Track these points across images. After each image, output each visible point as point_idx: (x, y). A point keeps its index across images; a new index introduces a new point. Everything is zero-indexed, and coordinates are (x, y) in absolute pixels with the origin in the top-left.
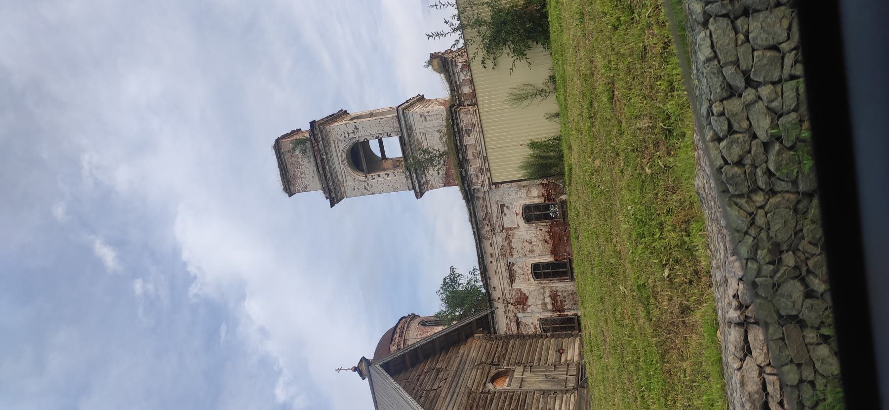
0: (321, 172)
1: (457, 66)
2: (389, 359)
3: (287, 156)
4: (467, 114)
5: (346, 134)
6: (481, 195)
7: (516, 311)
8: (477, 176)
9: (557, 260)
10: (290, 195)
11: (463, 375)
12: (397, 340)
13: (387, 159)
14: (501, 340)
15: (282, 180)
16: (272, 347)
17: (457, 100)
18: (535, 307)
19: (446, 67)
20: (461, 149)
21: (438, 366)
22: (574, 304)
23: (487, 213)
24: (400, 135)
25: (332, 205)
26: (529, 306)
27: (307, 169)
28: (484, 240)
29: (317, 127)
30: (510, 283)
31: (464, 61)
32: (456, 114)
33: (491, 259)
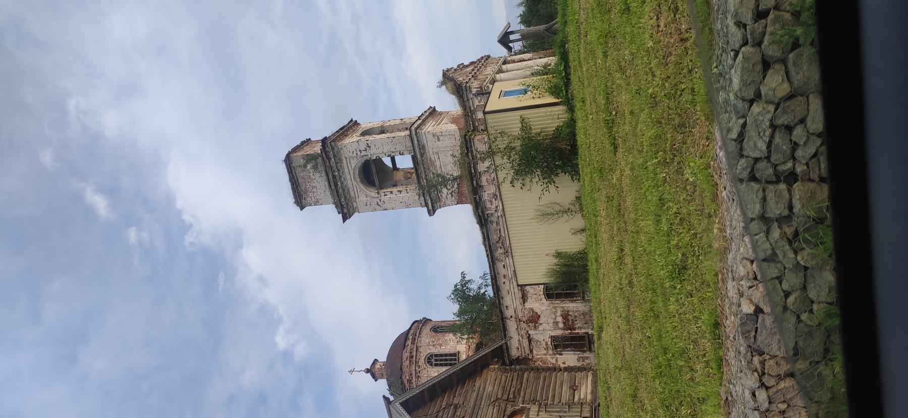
0: (333, 187)
2: (408, 397)
3: (298, 170)
5: (358, 151)
6: (494, 219)
7: (528, 329)
10: (302, 209)
11: (480, 413)
12: (409, 347)
13: (398, 169)
14: (516, 372)
15: (293, 194)
16: (271, 296)
17: (471, 125)
18: (547, 325)
20: (475, 176)
21: (455, 402)
22: (585, 323)
23: (500, 236)
24: (413, 154)
25: (344, 220)
26: (541, 324)
27: (318, 183)
28: (497, 262)
29: (329, 145)
30: (522, 303)
31: (478, 86)
32: (470, 142)
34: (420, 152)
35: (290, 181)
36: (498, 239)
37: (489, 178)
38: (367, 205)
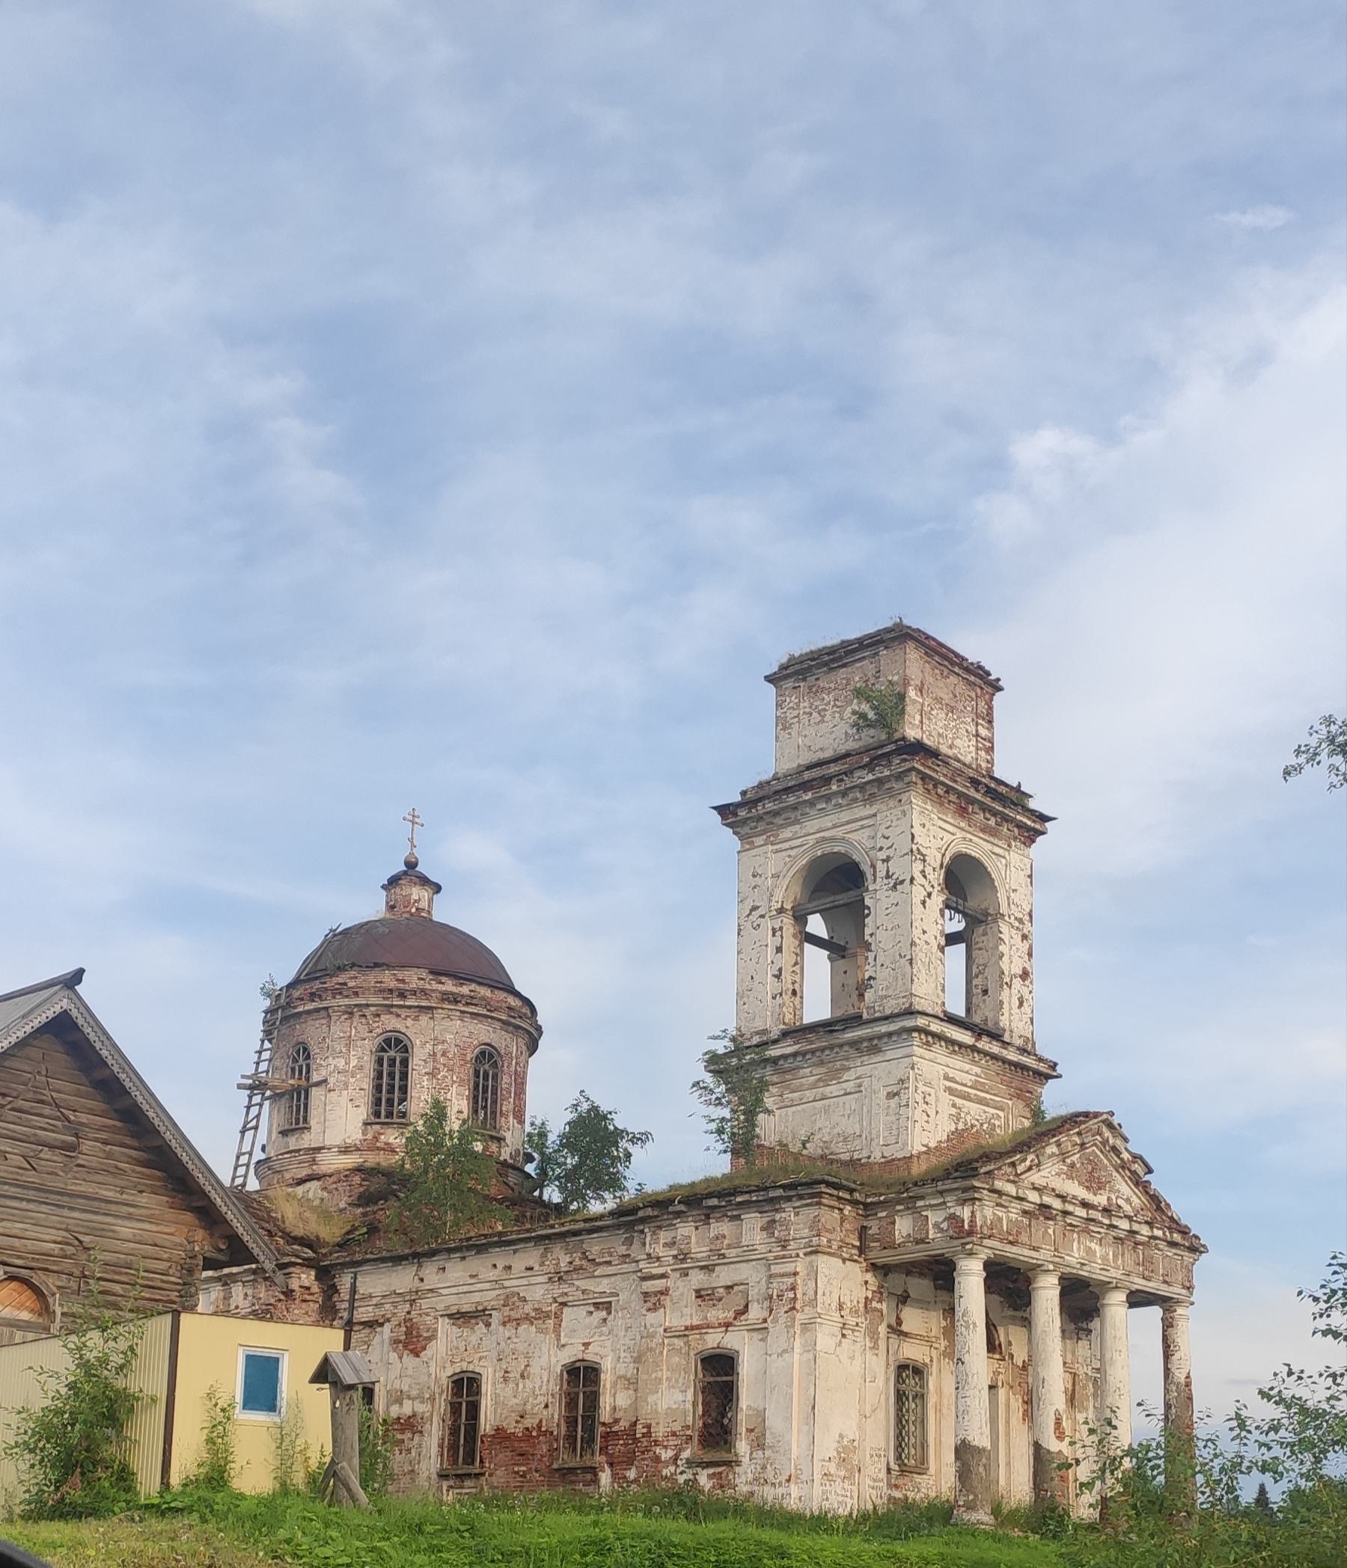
0: (807, 776)
1: (963, 1202)
4: (811, 1228)
6: (635, 1251)
7: (394, 1322)
8: (672, 1244)
9: (482, 1442)
11: (44, 1208)
12: (435, 986)
19: (956, 1171)
25: (725, 811)
29: (908, 765)
30: (449, 1312)
32: (812, 1196)
33: (500, 1267)
34: (861, 1040)
35: (845, 644)
36: (590, 1257)
37: (726, 1242)
38: (754, 876)
